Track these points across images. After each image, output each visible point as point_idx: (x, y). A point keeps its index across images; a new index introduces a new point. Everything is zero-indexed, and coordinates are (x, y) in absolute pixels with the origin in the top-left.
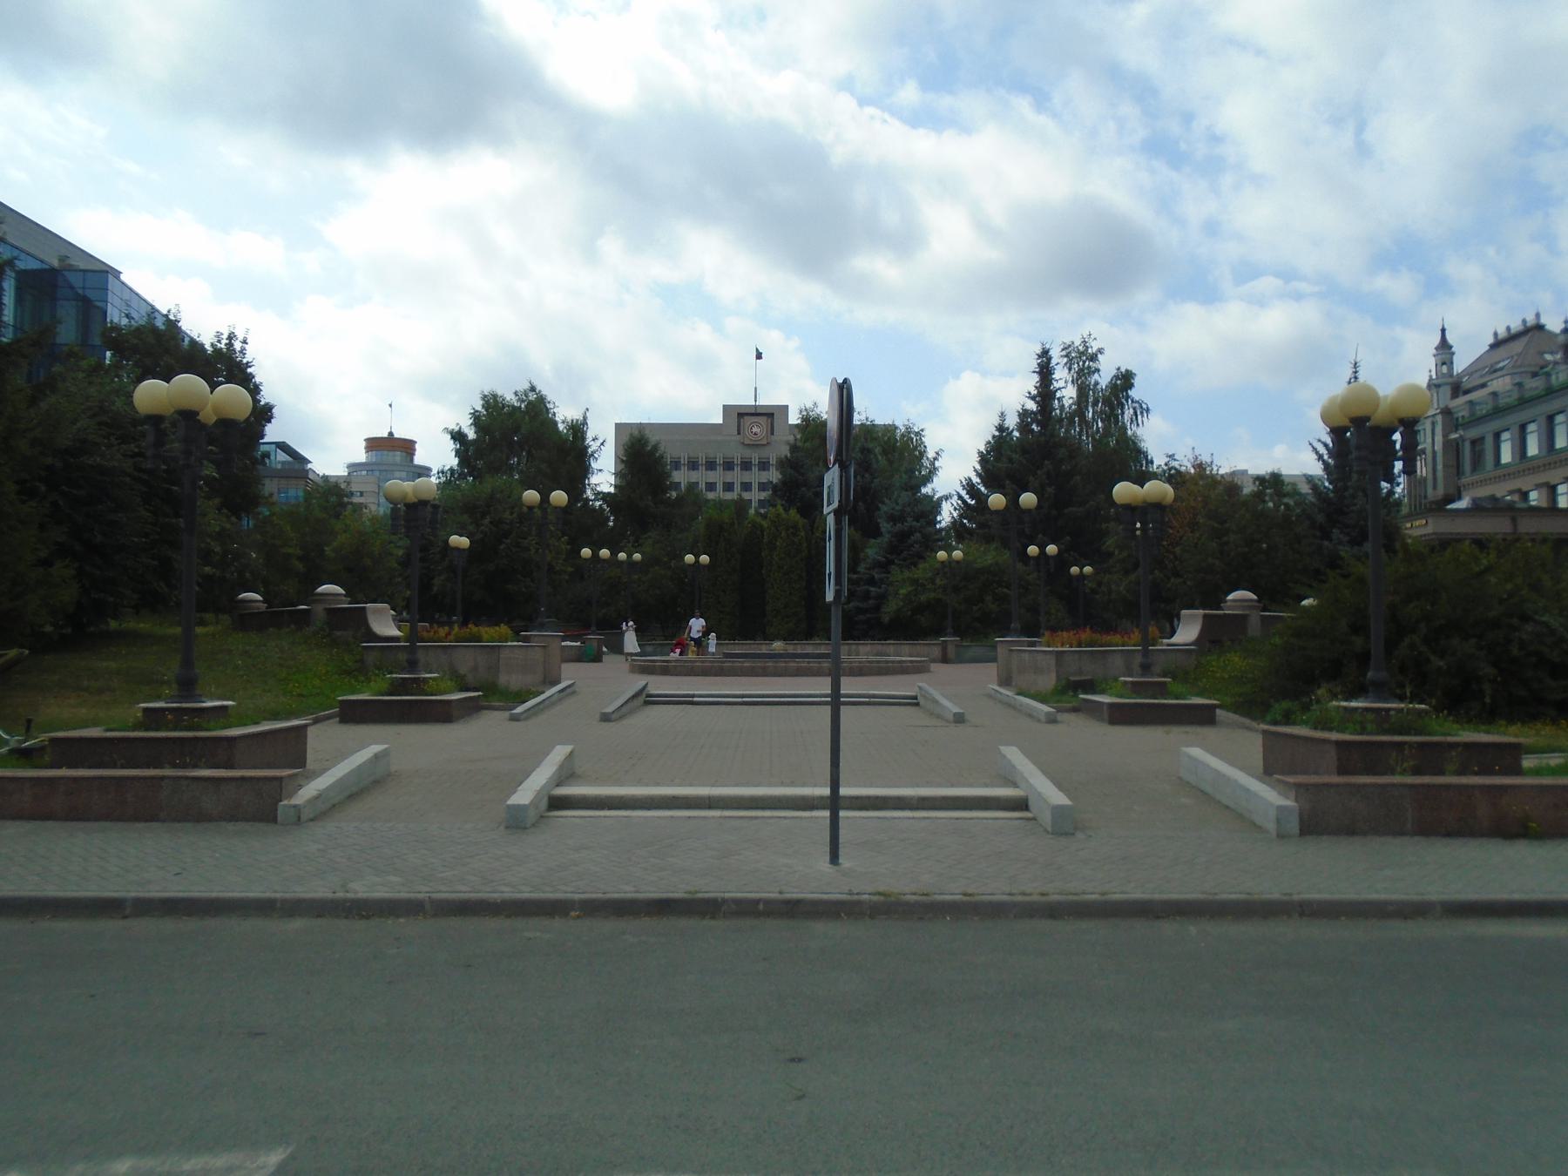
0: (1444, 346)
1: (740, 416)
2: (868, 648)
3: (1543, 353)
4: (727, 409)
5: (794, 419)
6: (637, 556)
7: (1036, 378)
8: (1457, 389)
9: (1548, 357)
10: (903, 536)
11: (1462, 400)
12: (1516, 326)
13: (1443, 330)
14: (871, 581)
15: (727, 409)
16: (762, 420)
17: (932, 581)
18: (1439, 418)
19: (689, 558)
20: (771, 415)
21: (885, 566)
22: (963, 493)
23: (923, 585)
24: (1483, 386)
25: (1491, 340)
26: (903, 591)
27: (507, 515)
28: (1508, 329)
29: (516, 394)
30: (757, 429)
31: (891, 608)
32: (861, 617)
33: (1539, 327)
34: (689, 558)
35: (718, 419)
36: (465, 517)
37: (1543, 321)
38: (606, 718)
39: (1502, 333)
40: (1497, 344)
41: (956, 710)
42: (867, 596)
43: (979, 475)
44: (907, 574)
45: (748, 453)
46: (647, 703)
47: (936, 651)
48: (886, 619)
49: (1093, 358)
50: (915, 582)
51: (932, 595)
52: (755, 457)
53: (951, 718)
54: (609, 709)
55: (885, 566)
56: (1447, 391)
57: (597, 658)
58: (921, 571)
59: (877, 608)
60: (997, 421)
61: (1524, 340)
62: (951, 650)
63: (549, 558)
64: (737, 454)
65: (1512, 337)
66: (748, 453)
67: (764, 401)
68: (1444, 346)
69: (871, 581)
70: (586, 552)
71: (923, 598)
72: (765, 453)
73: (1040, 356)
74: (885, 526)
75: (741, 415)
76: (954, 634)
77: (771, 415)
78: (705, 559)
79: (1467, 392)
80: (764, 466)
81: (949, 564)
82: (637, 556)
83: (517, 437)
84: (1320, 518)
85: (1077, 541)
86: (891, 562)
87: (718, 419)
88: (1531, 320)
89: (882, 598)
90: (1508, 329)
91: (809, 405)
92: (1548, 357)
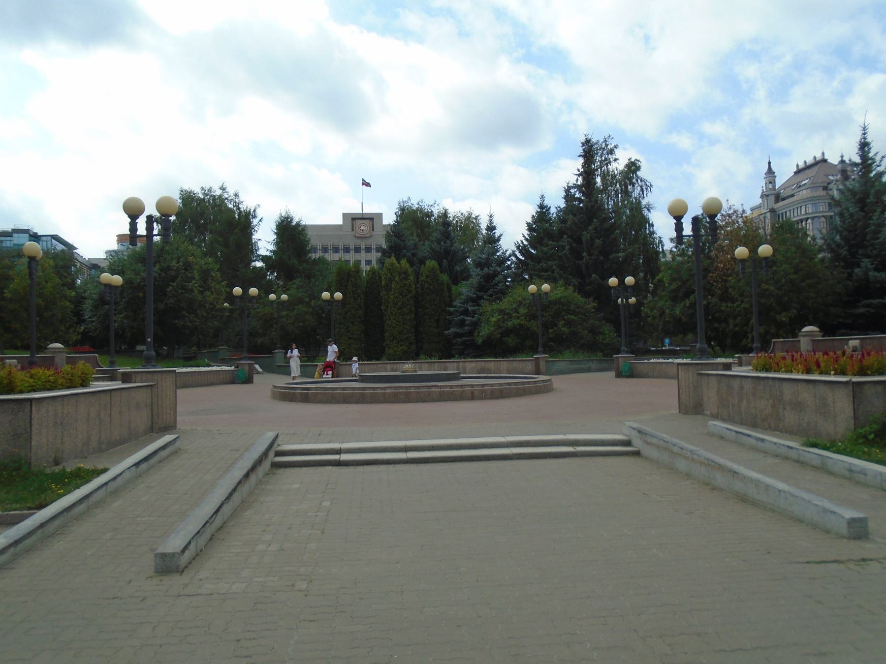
0: (770, 172)
1: (353, 219)
2: (473, 365)
3: (827, 176)
4: (345, 216)
5: (389, 219)
6: (284, 297)
7: (581, 161)
8: (778, 198)
9: (831, 178)
10: (489, 278)
11: (781, 204)
12: (810, 161)
13: (769, 163)
14: (466, 312)
15: (345, 216)
16: (367, 222)
17: (516, 311)
18: (768, 215)
19: (326, 295)
20: (372, 219)
21: (476, 301)
22: (517, 253)
23: (508, 314)
24: (793, 196)
25: (795, 169)
26: (493, 319)
27: (174, 263)
28: (805, 162)
29: (202, 188)
30: (364, 227)
31: (485, 331)
32: (459, 340)
33: (824, 161)
34: (326, 295)
35: (339, 221)
36: (140, 265)
37: (826, 157)
38: (167, 566)
39: (801, 165)
40: (799, 172)
41: (849, 514)
42: (462, 323)
43: (526, 239)
44: (495, 306)
45: (358, 242)
46: (276, 466)
47: (530, 366)
48: (480, 341)
49: (611, 152)
50: (501, 312)
51: (517, 322)
52: (363, 244)
53: (844, 529)
54: (174, 544)
55: (476, 301)
56: (772, 198)
57: (249, 380)
58: (505, 304)
59: (471, 333)
60: (538, 202)
61: (816, 168)
62: (542, 364)
63: (211, 299)
64: (352, 243)
65: (808, 167)
66: (358, 242)
67: (367, 210)
68: (770, 172)
69: (466, 312)
70: (355, 358)
71: (510, 324)
72: (368, 242)
73: (583, 144)
74: (475, 272)
75: (354, 219)
76: (544, 352)
77: (372, 219)
78: (338, 295)
79: (783, 199)
80: (368, 250)
81: (539, 295)
82: (284, 297)
83: (206, 225)
84: (844, 252)
85: (597, 283)
86: (481, 298)
87: (339, 221)
88: (819, 157)
89: (475, 325)
90: (805, 162)
91: (405, 199)
92: (831, 178)
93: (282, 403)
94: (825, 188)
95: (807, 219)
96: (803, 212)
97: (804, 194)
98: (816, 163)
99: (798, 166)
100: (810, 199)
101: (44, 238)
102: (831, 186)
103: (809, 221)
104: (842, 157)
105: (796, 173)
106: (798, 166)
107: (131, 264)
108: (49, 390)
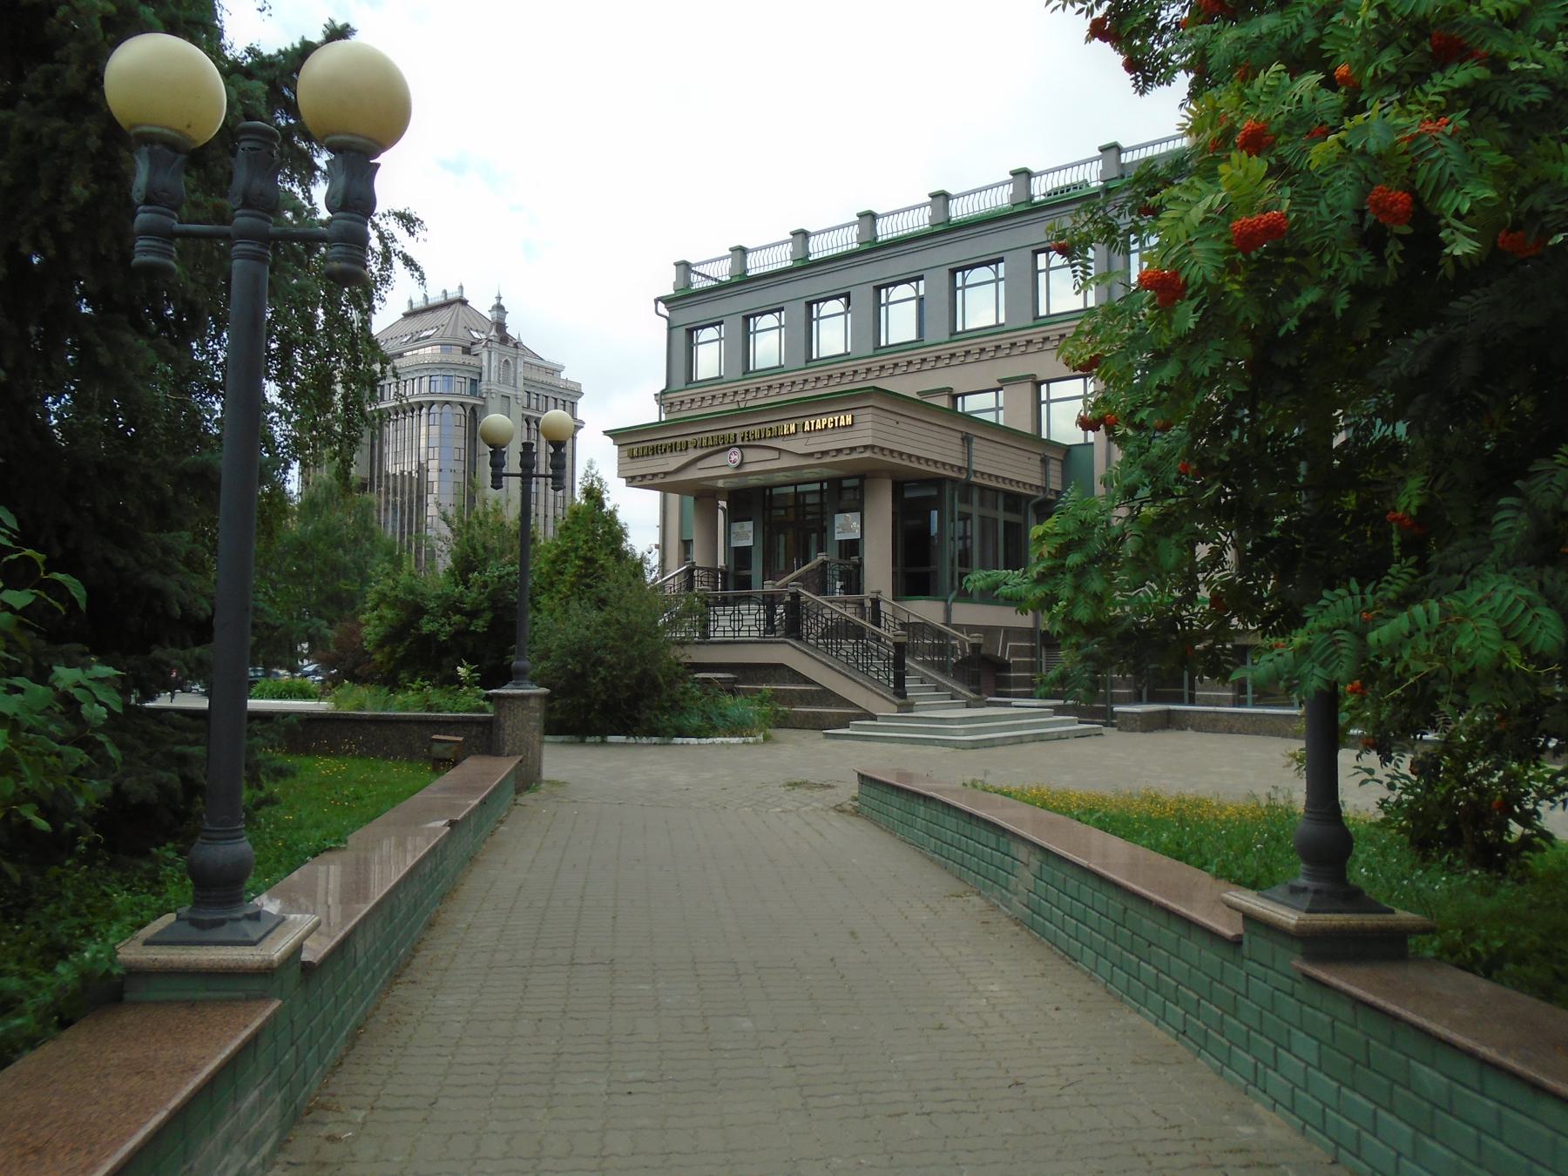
25: (406, 309)
33: (464, 302)
37: (466, 296)
88: (453, 293)
92: (475, 334)
93: (1148, 735)
94: (467, 351)
95: (433, 403)
96: (425, 389)
97: (428, 353)
98: (447, 304)
99: (411, 302)
100: (441, 366)
101: (91, 124)
102: (476, 349)
103: (435, 408)
104: (499, 298)
105: (406, 315)
106: (411, 302)
107: (1346, 279)
108: (280, 697)
